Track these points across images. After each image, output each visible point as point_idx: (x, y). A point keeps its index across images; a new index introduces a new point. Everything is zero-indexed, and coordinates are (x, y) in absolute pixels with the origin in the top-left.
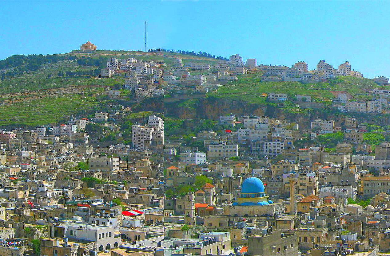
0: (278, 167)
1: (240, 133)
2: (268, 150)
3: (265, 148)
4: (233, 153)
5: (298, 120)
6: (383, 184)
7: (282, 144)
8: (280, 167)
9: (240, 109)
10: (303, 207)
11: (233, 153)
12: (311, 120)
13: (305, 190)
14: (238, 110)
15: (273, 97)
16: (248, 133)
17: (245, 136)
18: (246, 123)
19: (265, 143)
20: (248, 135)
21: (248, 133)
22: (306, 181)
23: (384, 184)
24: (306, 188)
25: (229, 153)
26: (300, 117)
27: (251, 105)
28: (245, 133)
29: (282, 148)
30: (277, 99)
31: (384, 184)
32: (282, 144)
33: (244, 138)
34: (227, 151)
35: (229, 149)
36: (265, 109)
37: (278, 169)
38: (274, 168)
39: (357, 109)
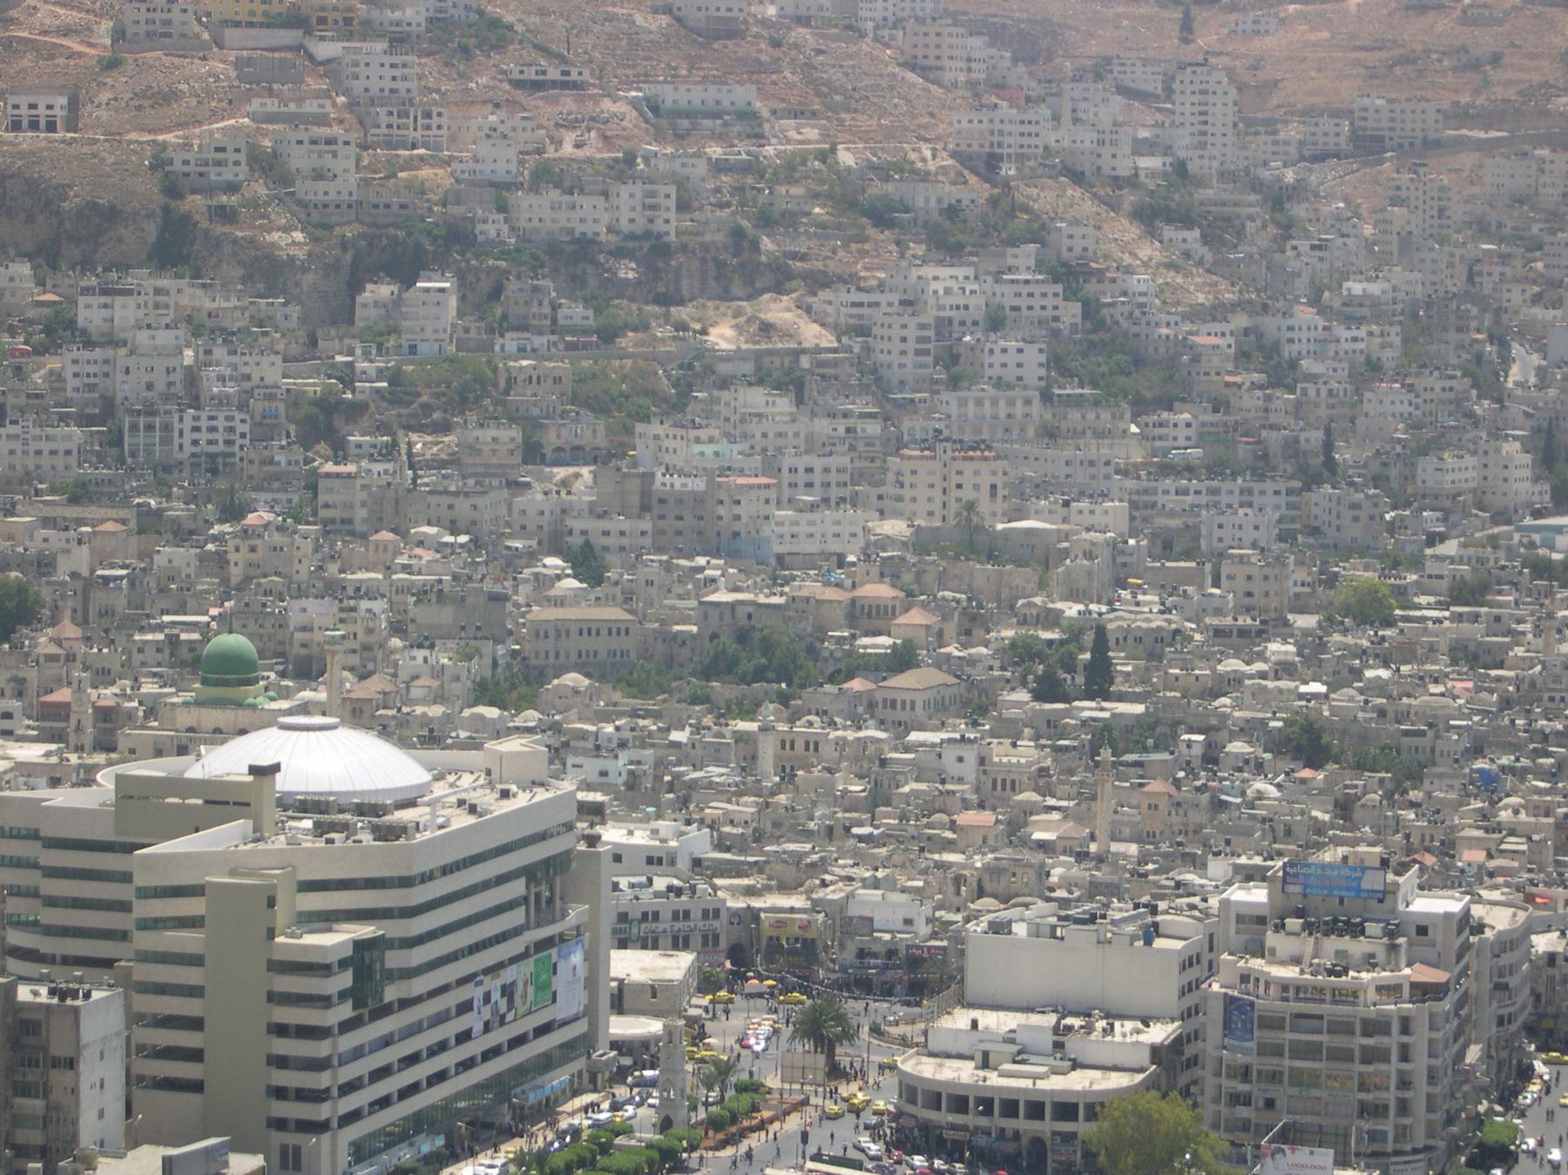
0: (253, 549)
1: (76, 369)
2: (187, 441)
3: (176, 434)
4: (60, 461)
5: (297, 284)
6: (594, 632)
7: (243, 421)
8: (259, 550)
9: (41, 218)
10: (354, 711)
11: (60, 461)
12: (355, 287)
13: (354, 651)
14: (30, 219)
15: (186, 169)
16: (106, 368)
17: (96, 380)
18: (88, 313)
19: (177, 416)
20: (106, 375)
21: (106, 368)
22: (359, 629)
23: (598, 633)
24: (355, 645)
25: (46, 461)
26: (305, 270)
27: (94, 207)
28: (92, 369)
29: (243, 435)
30: (201, 175)
31: (598, 633)
32: (243, 421)
33: (91, 388)
34: (38, 452)
35: (46, 447)
36: (152, 229)
37: (252, 556)
38: (237, 550)
39: (563, 223)
